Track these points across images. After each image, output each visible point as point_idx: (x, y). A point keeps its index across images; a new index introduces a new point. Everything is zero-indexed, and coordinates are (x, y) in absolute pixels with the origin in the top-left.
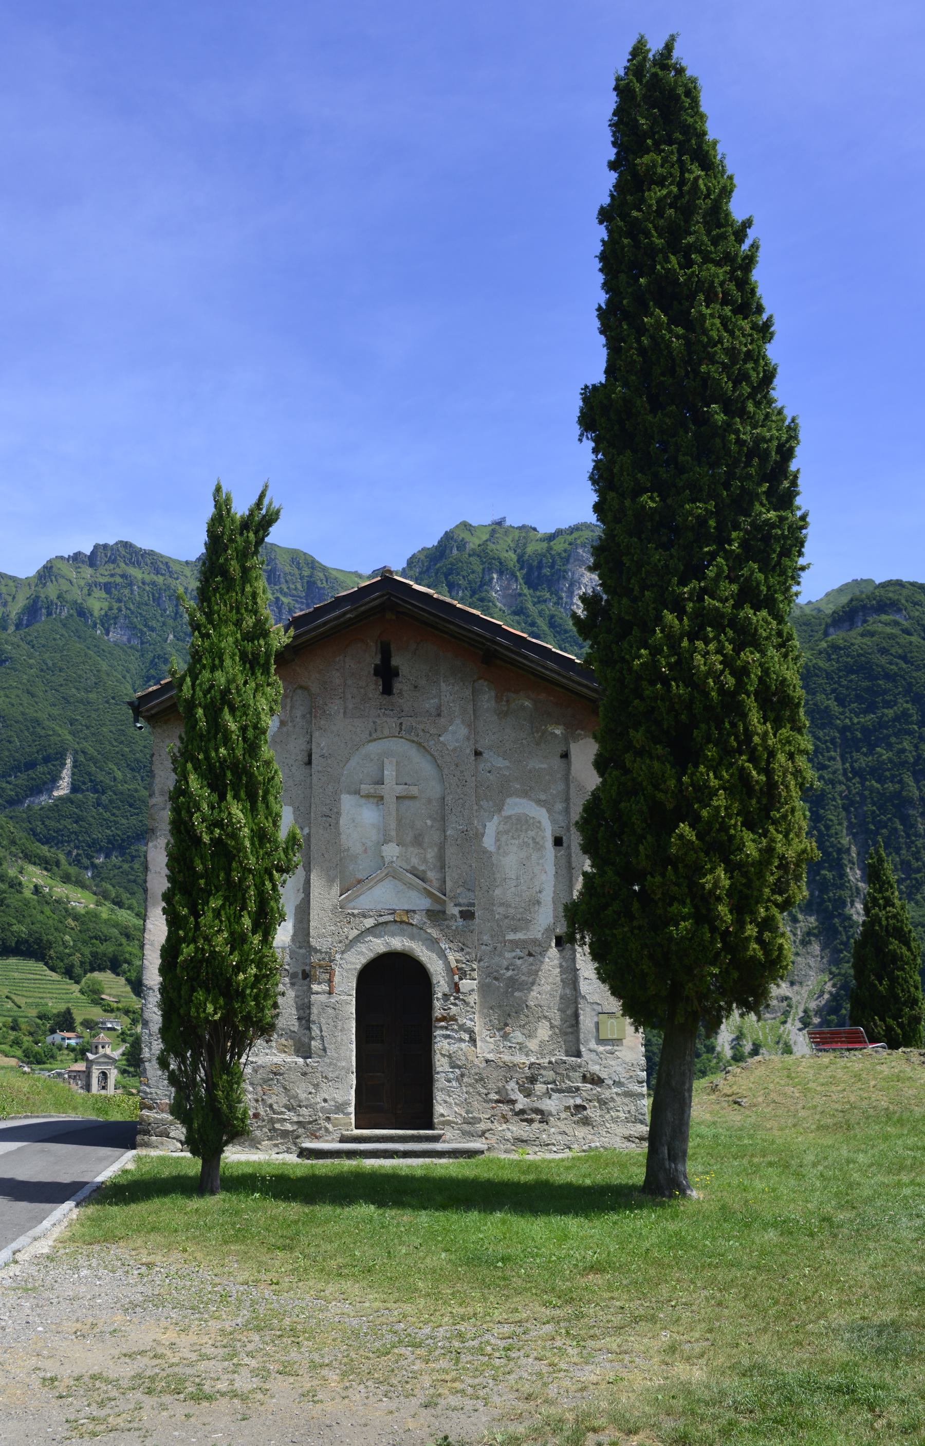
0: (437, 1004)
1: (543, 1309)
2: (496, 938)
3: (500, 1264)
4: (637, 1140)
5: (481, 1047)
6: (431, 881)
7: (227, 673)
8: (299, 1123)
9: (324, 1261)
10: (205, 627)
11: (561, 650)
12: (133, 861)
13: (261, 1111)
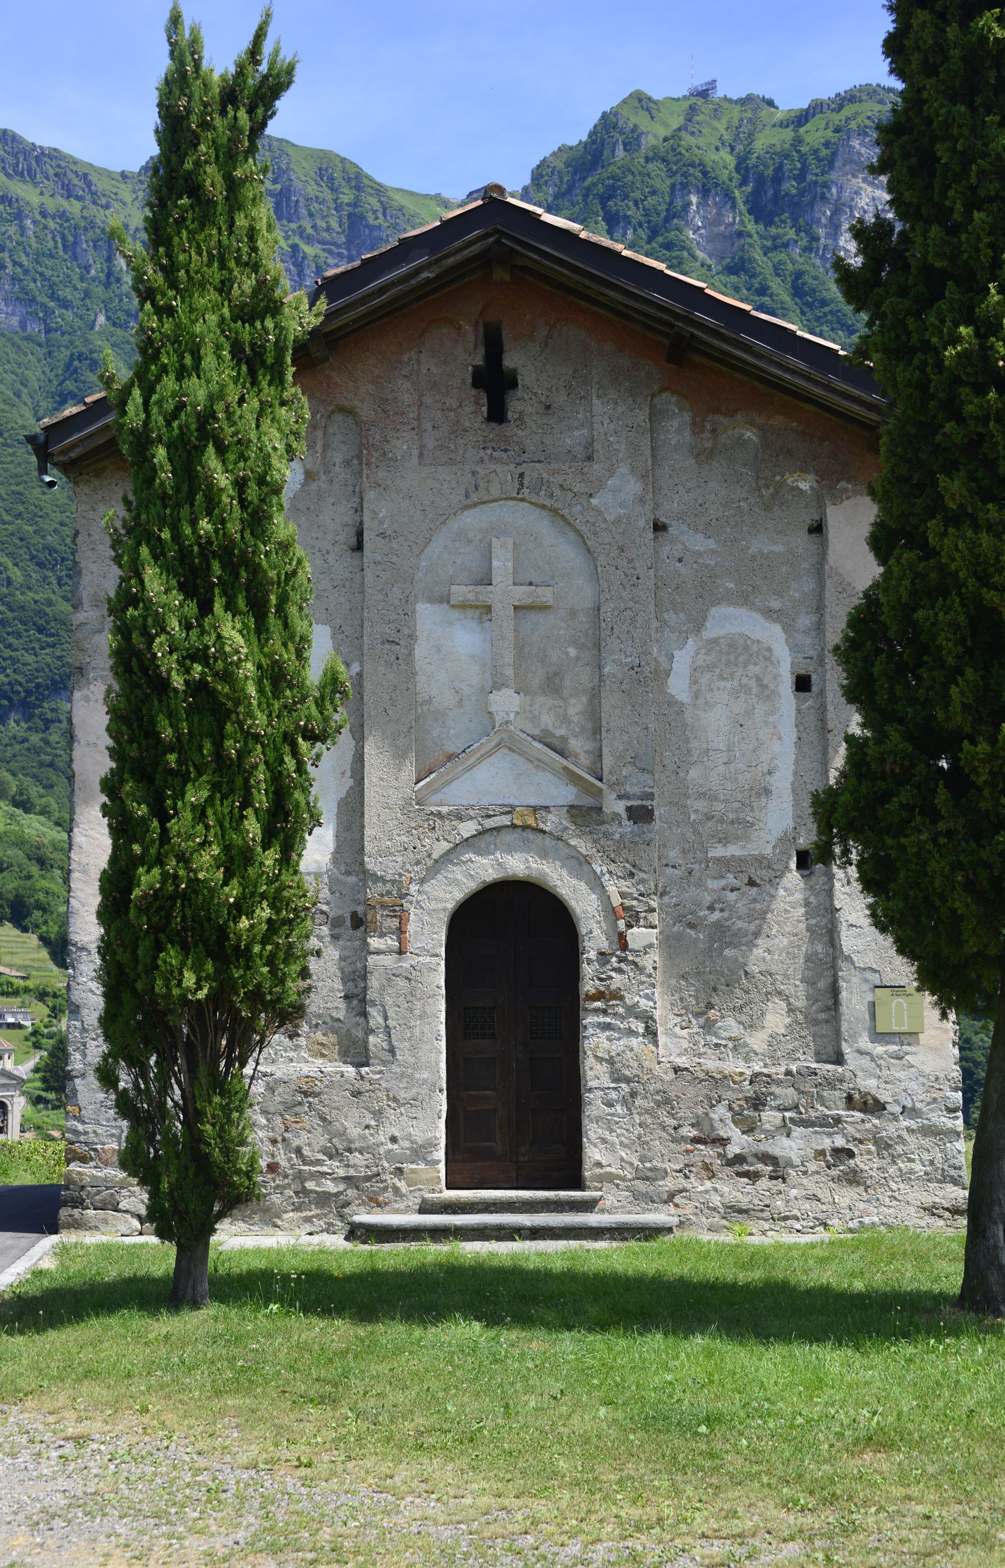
0: (588, 970)
1: (783, 1514)
2: (691, 855)
3: (703, 1429)
4: (947, 1214)
5: (666, 1045)
6: (576, 756)
7: (208, 382)
8: (347, 1179)
9: (391, 1421)
10: (164, 295)
11: (812, 333)
12: (47, 728)
13: (282, 1160)
